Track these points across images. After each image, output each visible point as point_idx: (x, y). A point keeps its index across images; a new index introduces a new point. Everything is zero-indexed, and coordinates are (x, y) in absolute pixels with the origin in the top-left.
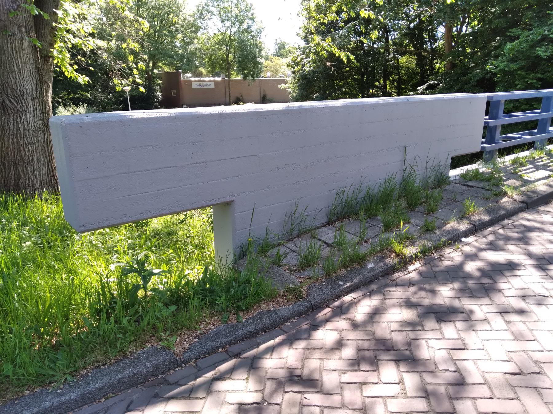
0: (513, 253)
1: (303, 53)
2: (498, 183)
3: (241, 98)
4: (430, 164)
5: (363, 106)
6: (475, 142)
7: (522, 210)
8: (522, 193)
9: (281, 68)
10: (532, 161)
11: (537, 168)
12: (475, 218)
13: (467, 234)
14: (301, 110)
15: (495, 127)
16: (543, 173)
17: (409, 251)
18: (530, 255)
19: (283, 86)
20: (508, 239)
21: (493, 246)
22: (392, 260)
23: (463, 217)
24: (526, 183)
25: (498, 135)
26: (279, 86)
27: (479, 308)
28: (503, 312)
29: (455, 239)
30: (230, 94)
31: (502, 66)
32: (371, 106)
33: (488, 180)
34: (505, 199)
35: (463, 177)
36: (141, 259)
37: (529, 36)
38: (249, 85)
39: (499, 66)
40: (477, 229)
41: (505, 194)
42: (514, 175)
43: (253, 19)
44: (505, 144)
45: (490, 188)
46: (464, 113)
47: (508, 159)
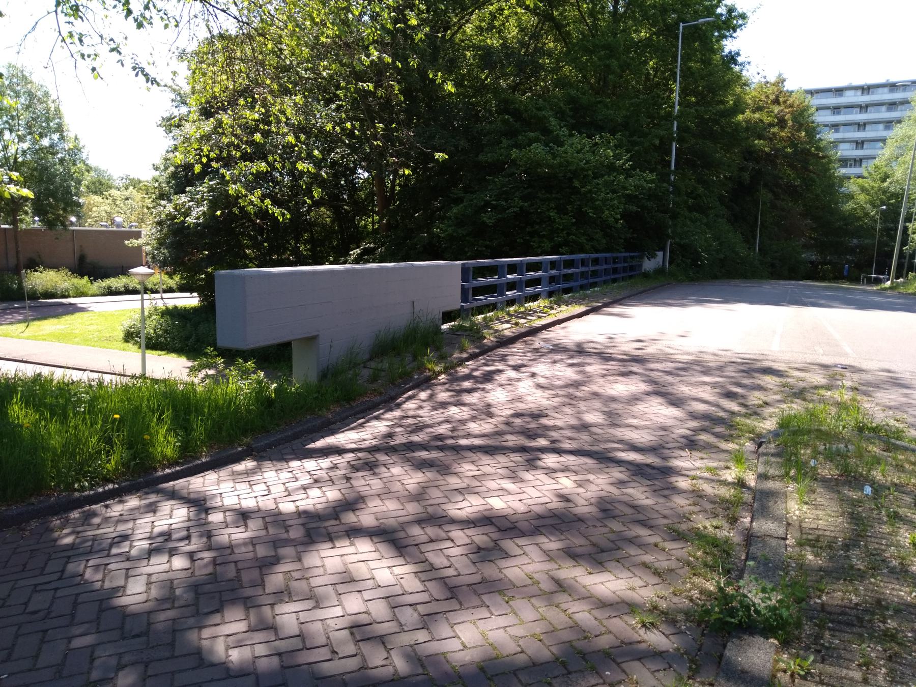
0: (499, 366)
1: (192, 200)
2: (478, 331)
3: (38, 260)
4: (429, 318)
5: (270, 274)
6: (455, 303)
7: (498, 347)
8: (496, 337)
9: (91, 210)
10: (498, 319)
11: (502, 323)
12: (470, 351)
13: (468, 360)
14: (354, 270)
15: (468, 289)
16: (507, 326)
17: (438, 369)
18: (509, 366)
19: (135, 242)
20: (494, 361)
21: (486, 365)
22: (428, 374)
23: (462, 350)
24: (497, 331)
25: (470, 298)
26: (126, 242)
27: (488, 386)
28: (501, 386)
29: (462, 362)
30: (18, 252)
31: (450, 230)
32: (405, 268)
33: (471, 330)
34: (486, 341)
35: (451, 329)
36: (820, 140)
37: (472, 200)
38: (57, 238)
39: (446, 230)
40: (473, 357)
41: (485, 338)
42: (488, 327)
43: (60, 129)
44: (476, 303)
45: (475, 334)
46: (437, 280)
47: (480, 317)
